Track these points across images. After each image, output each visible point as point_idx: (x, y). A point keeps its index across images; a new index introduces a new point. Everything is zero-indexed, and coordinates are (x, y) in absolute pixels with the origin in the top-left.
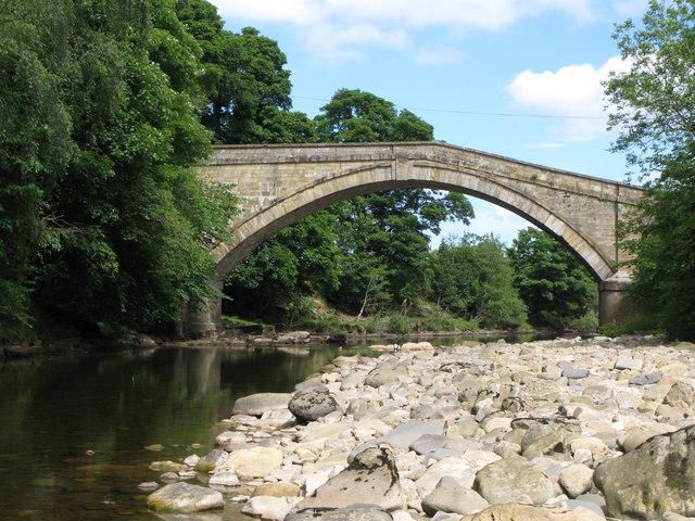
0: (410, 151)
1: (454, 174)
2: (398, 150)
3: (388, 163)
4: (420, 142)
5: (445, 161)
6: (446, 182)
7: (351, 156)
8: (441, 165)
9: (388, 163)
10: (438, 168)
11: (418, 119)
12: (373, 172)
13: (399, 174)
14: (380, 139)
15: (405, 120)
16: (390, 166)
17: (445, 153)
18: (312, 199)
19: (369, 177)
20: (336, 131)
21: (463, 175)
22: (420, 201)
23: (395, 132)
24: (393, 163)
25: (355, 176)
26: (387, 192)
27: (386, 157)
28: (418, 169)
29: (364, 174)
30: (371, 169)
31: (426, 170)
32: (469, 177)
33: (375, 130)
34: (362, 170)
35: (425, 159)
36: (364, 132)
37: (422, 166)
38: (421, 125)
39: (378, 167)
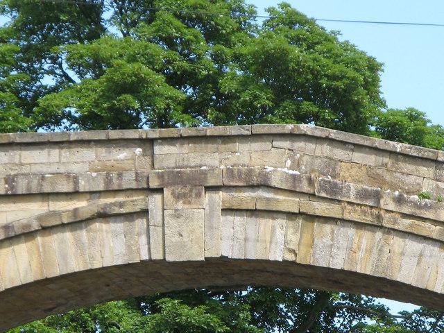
0: (213, 160)
1: (366, 239)
2: (168, 155)
3: (137, 202)
4: (245, 130)
5: (333, 194)
6: (338, 263)
7: (9, 180)
8: (320, 208)
9: (137, 202)
10: (311, 218)
11: (329, 39)
12: (83, 234)
13: (172, 239)
14: (193, 108)
15: (278, 42)
16: (144, 213)
17: (331, 162)
18: (277, 255)
19: (71, 249)
20: (48, 81)
21: (397, 242)
22: (338, 322)
23: (244, 84)
24: (155, 202)
25: (22, 248)
26: (227, 291)
27: (129, 181)
28: (238, 220)
29: (54, 240)
30: (77, 223)
31: (266, 224)
32: (414, 246)
33: (176, 80)
34: (46, 230)
35: (267, 187)
36: (135, 87)
37: (253, 212)
38: (336, 58)
39: (103, 216)
